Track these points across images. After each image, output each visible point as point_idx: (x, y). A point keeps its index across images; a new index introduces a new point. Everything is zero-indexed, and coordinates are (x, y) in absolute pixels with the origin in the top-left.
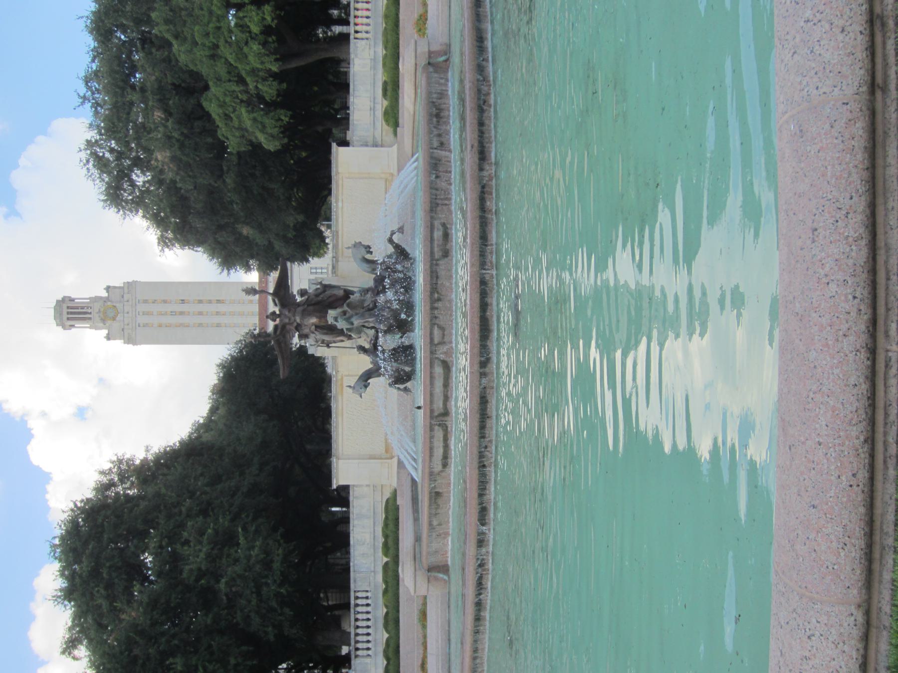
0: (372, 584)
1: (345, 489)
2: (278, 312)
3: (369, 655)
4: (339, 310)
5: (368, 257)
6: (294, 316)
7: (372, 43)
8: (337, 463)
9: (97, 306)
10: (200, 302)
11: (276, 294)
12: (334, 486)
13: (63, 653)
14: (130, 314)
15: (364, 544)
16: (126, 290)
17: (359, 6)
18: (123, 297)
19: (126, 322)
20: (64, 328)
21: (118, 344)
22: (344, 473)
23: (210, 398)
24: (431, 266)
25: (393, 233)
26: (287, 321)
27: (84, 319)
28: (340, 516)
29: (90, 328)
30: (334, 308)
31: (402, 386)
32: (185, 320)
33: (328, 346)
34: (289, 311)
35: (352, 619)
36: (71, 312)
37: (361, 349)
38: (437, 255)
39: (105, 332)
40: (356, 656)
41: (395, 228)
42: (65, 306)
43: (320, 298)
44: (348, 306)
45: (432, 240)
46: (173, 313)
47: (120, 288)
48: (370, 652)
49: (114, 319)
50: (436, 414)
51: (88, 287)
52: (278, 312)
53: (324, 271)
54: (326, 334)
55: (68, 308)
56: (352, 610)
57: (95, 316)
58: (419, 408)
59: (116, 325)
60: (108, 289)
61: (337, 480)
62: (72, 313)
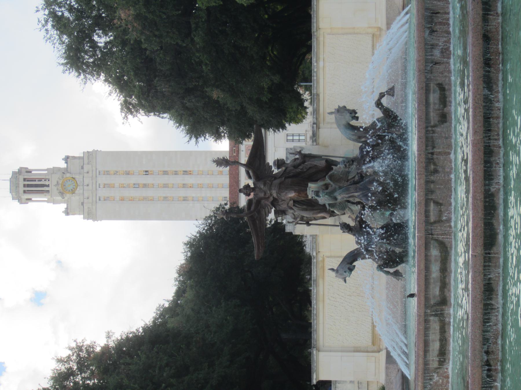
2: (252, 186)
4: (320, 183)
5: (354, 123)
6: (270, 189)
8: (317, 356)
10: (165, 173)
11: (249, 165)
12: (314, 382)
18: (82, 168)
19: (86, 195)
20: (21, 202)
23: (176, 280)
24: (427, 131)
25: (382, 95)
26: (262, 195)
27: (42, 192)
29: (48, 202)
30: (315, 181)
31: (392, 270)
33: (308, 224)
34: (265, 184)
36: (29, 185)
37: (346, 227)
38: (434, 117)
39: (63, 206)
41: (384, 89)
42: (21, 178)
43: (298, 170)
44: (331, 178)
45: (427, 104)
46: (136, 186)
49: (73, 192)
50: (432, 302)
51: (45, 157)
52: (252, 186)
53: (301, 138)
54: (306, 210)
55: (25, 180)
57: (53, 188)
58: (412, 296)
59: (75, 199)
60: (67, 159)
62: (29, 186)
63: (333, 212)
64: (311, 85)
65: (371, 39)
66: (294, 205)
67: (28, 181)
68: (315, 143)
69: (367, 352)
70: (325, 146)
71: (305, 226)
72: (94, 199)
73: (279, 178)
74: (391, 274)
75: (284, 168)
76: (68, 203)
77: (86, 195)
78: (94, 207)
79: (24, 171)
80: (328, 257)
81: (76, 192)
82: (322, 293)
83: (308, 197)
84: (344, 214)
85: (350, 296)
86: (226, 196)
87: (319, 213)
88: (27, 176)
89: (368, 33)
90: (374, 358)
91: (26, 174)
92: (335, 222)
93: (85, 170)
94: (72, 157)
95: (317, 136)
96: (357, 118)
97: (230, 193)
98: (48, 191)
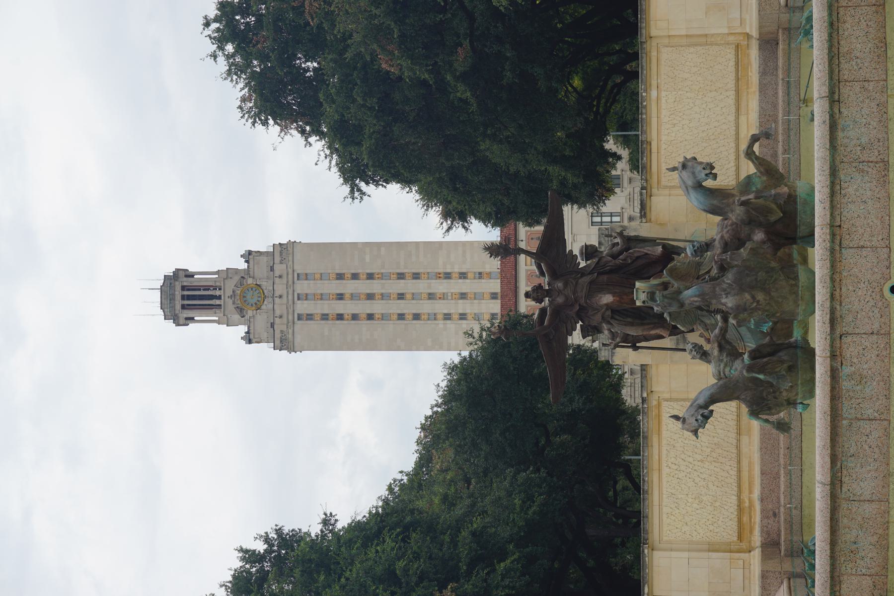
4: (654, 282)
5: (709, 183)
10: (401, 276)
14: (284, 300)
16: (277, 259)
18: (272, 269)
19: (278, 313)
23: (419, 442)
25: (755, 139)
26: (560, 300)
29: (219, 322)
30: (645, 278)
32: (377, 307)
33: (635, 348)
36: (187, 297)
39: (242, 329)
43: (619, 261)
44: (672, 273)
51: (213, 255)
54: (632, 324)
55: (183, 288)
59: (261, 321)
60: (249, 256)
62: (189, 297)
63: (675, 327)
64: (637, 136)
65: (733, 52)
66: (612, 318)
67: (188, 290)
68: (644, 220)
69: (731, 551)
70: (661, 224)
71: (630, 350)
72: (290, 317)
73: (589, 274)
74: (772, 423)
75: (595, 260)
76: (249, 324)
77: (278, 313)
78: (290, 331)
79: (182, 274)
80: (667, 400)
81: (263, 307)
82: (657, 457)
83: (634, 302)
84: (692, 331)
85: (702, 461)
86: (495, 312)
87: (653, 329)
88: (187, 282)
89: (728, 44)
90: (741, 562)
91: (185, 279)
92: (678, 344)
93: (277, 273)
94: (256, 252)
95: (648, 208)
96: (715, 176)
97: (502, 306)
98: (220, 305)
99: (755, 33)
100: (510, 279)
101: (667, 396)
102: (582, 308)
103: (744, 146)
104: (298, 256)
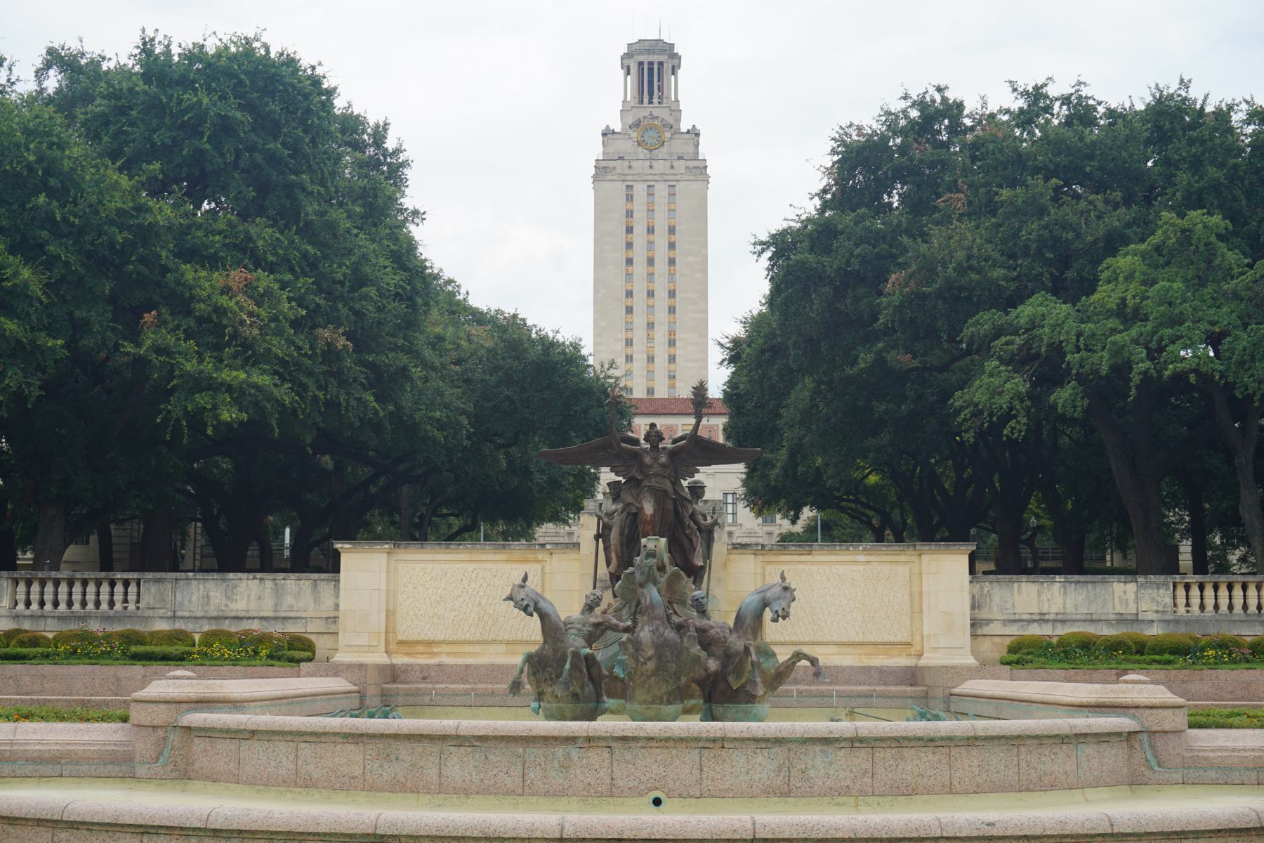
0: (147, 613)
1: (332, 565)
3: (16, 604)
4: (666, 557)
5: (768, 614)
7: (1169, 617)
9: (661, 113)
10: (672, 294)
13: (51, 51)
15: (228, 598)
16: (691, 164)
17: (1252, 592)
18: (680, 158)
19: (634, 164)
21: (596, 150)
22: (366, 569)
25: (813, 661)
28: (274, 545)
32: (639, 268)
33: (597, 537)
35: (86, 575)
36: (652, 68)
39: (617, 126)
40: (16, 582)
42: (663, 58)
43: (688, 521)
44: (675, 575)
47: (697, 153)
48: (21, 606)
51: (693, 95)
54: (621, 534)
55: (661, 64)
56: (103, 574)
60: (694, 133)
61: (347, 551)
62: (651, 70)
80: (543, 569)
88: (667, 68)
93: (676, 163)
99: (923, 662)
100: (669, 407)
101: (547, 570)
102: (639, 483)
103: (806, 650)
104: (694, 185)
